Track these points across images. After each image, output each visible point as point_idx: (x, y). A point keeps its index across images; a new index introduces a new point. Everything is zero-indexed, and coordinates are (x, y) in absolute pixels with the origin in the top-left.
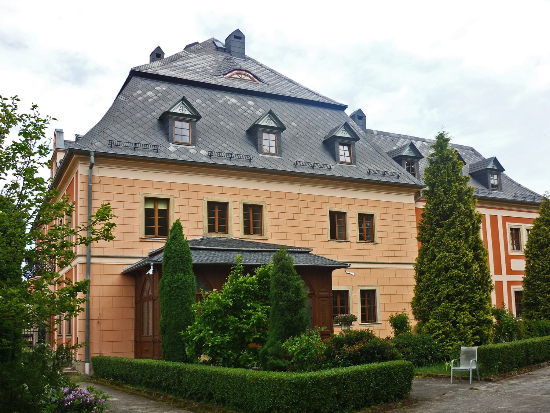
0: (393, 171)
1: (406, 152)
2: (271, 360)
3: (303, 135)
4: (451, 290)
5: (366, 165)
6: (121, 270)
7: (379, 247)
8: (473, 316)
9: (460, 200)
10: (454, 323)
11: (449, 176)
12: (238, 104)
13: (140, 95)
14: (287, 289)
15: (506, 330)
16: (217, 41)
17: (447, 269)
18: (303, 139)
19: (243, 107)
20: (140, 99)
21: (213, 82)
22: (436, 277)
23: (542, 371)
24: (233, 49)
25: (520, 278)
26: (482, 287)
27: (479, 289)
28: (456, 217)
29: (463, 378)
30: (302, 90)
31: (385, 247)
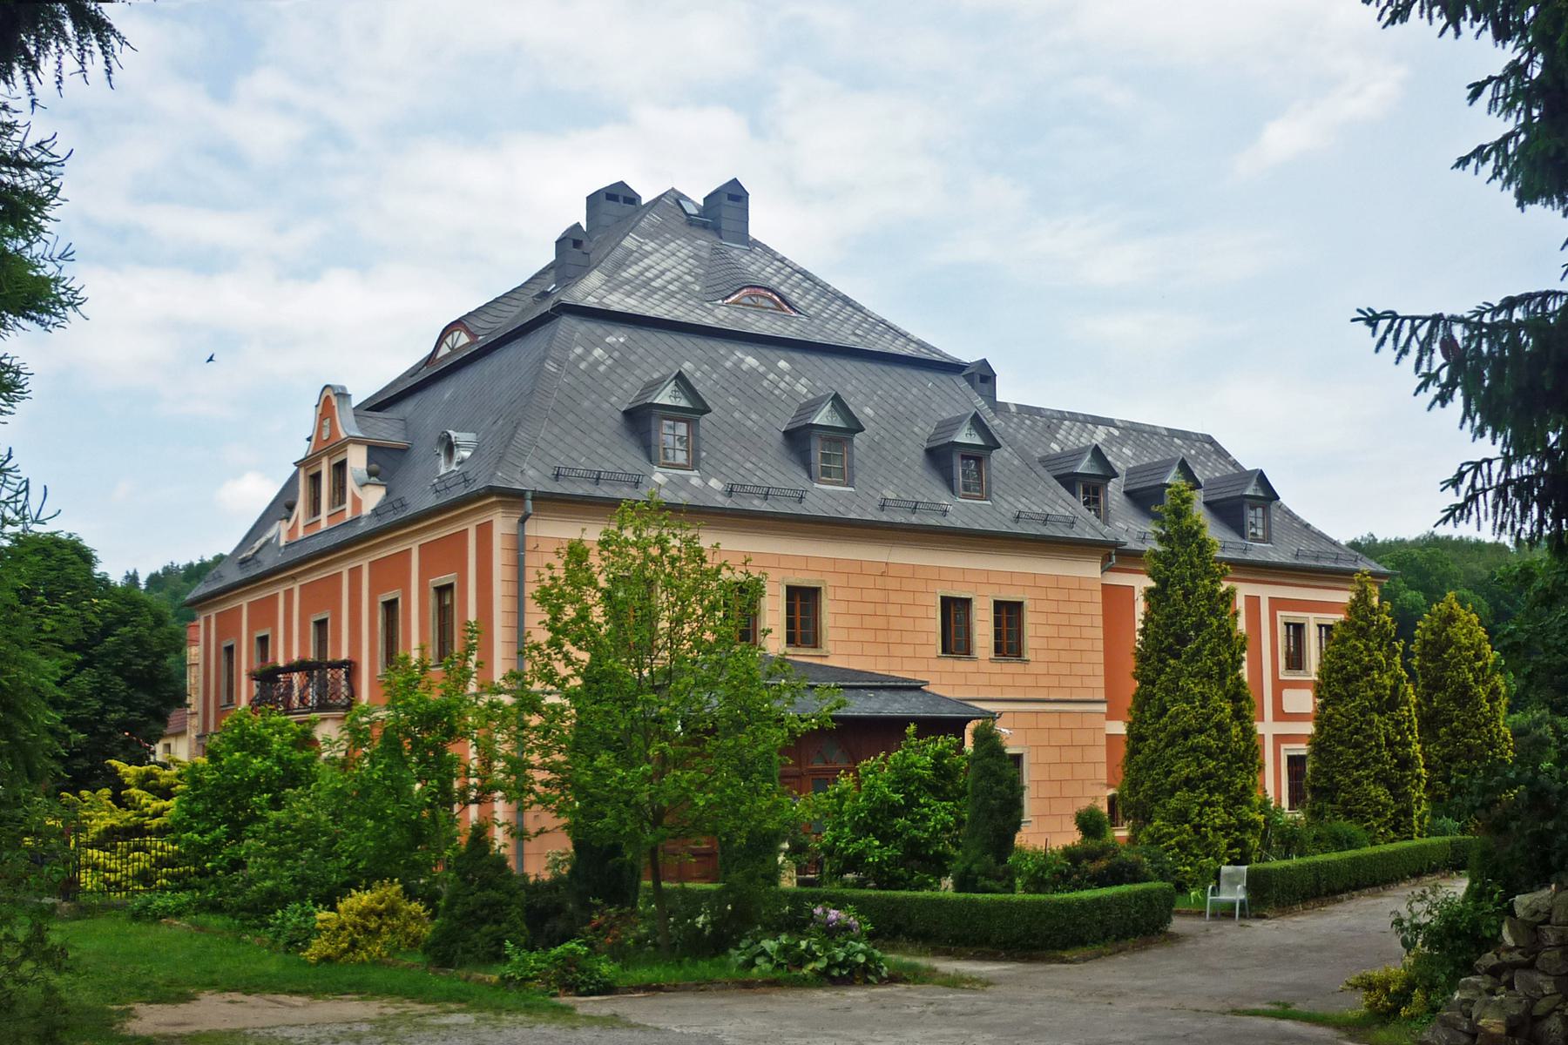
0: (1062, 511)
1: (1084, 466)
2: (982, 881)
3: (887, 436)
4: (1192, 770)
5: (1011, 499)
7: (1031, 668)
8: (1230, 814)
9: (1213, 612)
10: (1197, 828)
11: (1193, 566)
12: (762, 369)
13: (581, 358)
14: (999, 782)
15: (1290, 841)
16: (688, 199)
17: (1186, 734)
18: (888, 446)
19: (771, 376)
20: (583, 366)
21: (709, 321)
22: (1167, 746)
23: (1338, 907)
26: (1246, 766)
27: (1240, 769)
28: (1205, 642)
29: (1225, 913)
30: (874, 325)
31: (1041, 669)
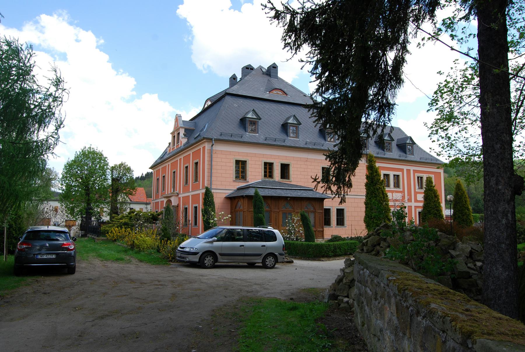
6: (225, 196)
24: (272, 74)
25: (421, 204)
